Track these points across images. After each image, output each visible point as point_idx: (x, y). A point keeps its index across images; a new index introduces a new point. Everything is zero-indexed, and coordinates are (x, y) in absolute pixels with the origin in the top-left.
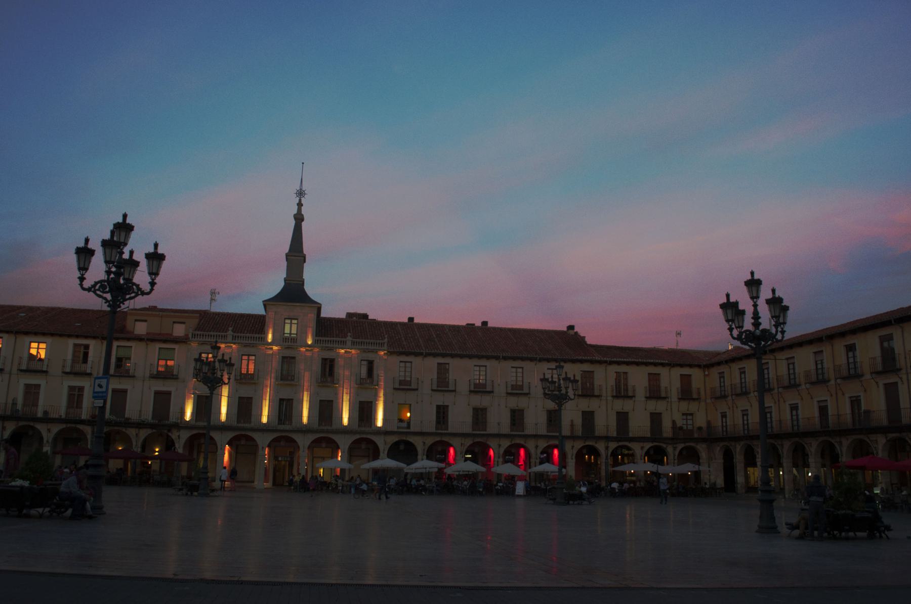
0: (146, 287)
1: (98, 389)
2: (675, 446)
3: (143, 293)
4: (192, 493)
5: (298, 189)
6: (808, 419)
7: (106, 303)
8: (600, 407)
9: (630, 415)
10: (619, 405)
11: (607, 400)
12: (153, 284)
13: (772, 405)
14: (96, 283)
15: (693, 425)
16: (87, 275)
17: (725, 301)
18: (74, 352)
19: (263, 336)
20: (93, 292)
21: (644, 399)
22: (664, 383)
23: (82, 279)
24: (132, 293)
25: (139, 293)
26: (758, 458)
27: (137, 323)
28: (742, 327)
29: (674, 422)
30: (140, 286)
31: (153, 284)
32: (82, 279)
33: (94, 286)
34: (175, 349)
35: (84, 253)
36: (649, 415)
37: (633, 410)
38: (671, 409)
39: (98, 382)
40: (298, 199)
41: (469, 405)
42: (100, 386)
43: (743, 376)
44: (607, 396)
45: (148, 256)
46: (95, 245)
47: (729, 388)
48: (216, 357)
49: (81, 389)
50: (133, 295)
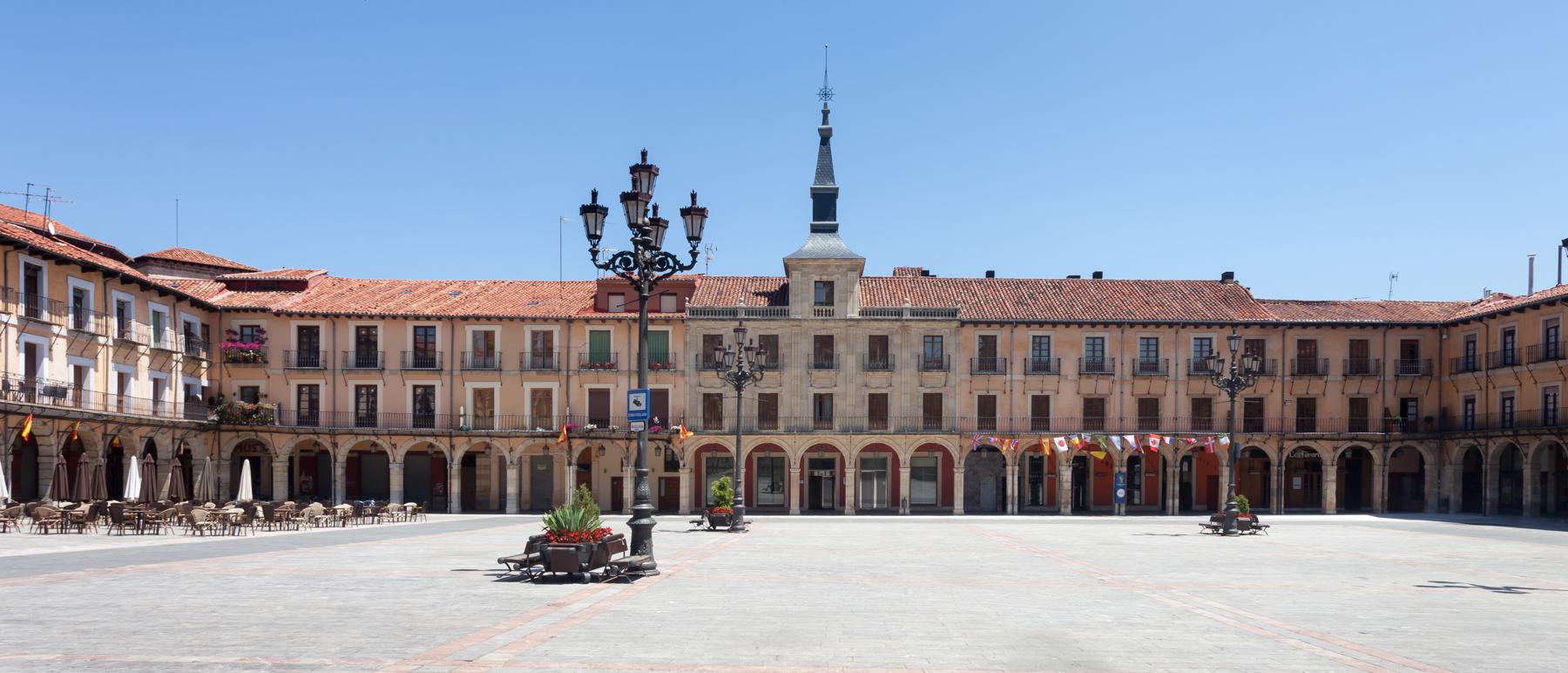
0: (686, 260)
1: (633, 407)
2: (1387, 445)
3: (682, 268)
4: (715, 528)
5: (822, 88)
6: (1530, 411)
7: (632, 284)
8: (1272, 391)
9: (1319, 402)
10: (1303, 387)
11: (1283, 380)
12: (694, 254)
13: (1560, 384)
14: (615, 257)
15: (1417, 414)
16: (601, 247)
17: (689, 205)
18: (534, 343)
19: (786, 308)
20: (612, 269)
21: (1340, 378)
22: (1375, 353)
23: (594, 253)
24: (666, 269)
25: (677, 267)
26: (1527, 463)
27: (611, 297)
28: (659, 249)
29: (1386, 412)
30: (678, 258)
31: (694, 254)
32: (594, 253)
33: (612, 261)
34: (435, 327)
35: (593, 211)
36: (1347, 402)
37: (1324, 394)
38: (1384, 392)
39: (632, 397)
40: (822, 102)
41: (1078, 393)
42: (637, 403)
43: (1509, 339)
44: (1283, 376)
45: (685, 212)
46: (610, 199)
47: (1484, 359)
48: (742, 344)
49: (548, 392)
50: (669, 271)
